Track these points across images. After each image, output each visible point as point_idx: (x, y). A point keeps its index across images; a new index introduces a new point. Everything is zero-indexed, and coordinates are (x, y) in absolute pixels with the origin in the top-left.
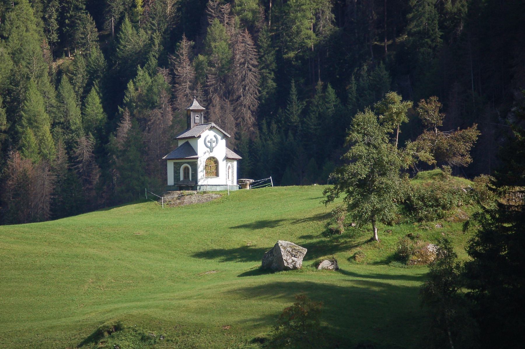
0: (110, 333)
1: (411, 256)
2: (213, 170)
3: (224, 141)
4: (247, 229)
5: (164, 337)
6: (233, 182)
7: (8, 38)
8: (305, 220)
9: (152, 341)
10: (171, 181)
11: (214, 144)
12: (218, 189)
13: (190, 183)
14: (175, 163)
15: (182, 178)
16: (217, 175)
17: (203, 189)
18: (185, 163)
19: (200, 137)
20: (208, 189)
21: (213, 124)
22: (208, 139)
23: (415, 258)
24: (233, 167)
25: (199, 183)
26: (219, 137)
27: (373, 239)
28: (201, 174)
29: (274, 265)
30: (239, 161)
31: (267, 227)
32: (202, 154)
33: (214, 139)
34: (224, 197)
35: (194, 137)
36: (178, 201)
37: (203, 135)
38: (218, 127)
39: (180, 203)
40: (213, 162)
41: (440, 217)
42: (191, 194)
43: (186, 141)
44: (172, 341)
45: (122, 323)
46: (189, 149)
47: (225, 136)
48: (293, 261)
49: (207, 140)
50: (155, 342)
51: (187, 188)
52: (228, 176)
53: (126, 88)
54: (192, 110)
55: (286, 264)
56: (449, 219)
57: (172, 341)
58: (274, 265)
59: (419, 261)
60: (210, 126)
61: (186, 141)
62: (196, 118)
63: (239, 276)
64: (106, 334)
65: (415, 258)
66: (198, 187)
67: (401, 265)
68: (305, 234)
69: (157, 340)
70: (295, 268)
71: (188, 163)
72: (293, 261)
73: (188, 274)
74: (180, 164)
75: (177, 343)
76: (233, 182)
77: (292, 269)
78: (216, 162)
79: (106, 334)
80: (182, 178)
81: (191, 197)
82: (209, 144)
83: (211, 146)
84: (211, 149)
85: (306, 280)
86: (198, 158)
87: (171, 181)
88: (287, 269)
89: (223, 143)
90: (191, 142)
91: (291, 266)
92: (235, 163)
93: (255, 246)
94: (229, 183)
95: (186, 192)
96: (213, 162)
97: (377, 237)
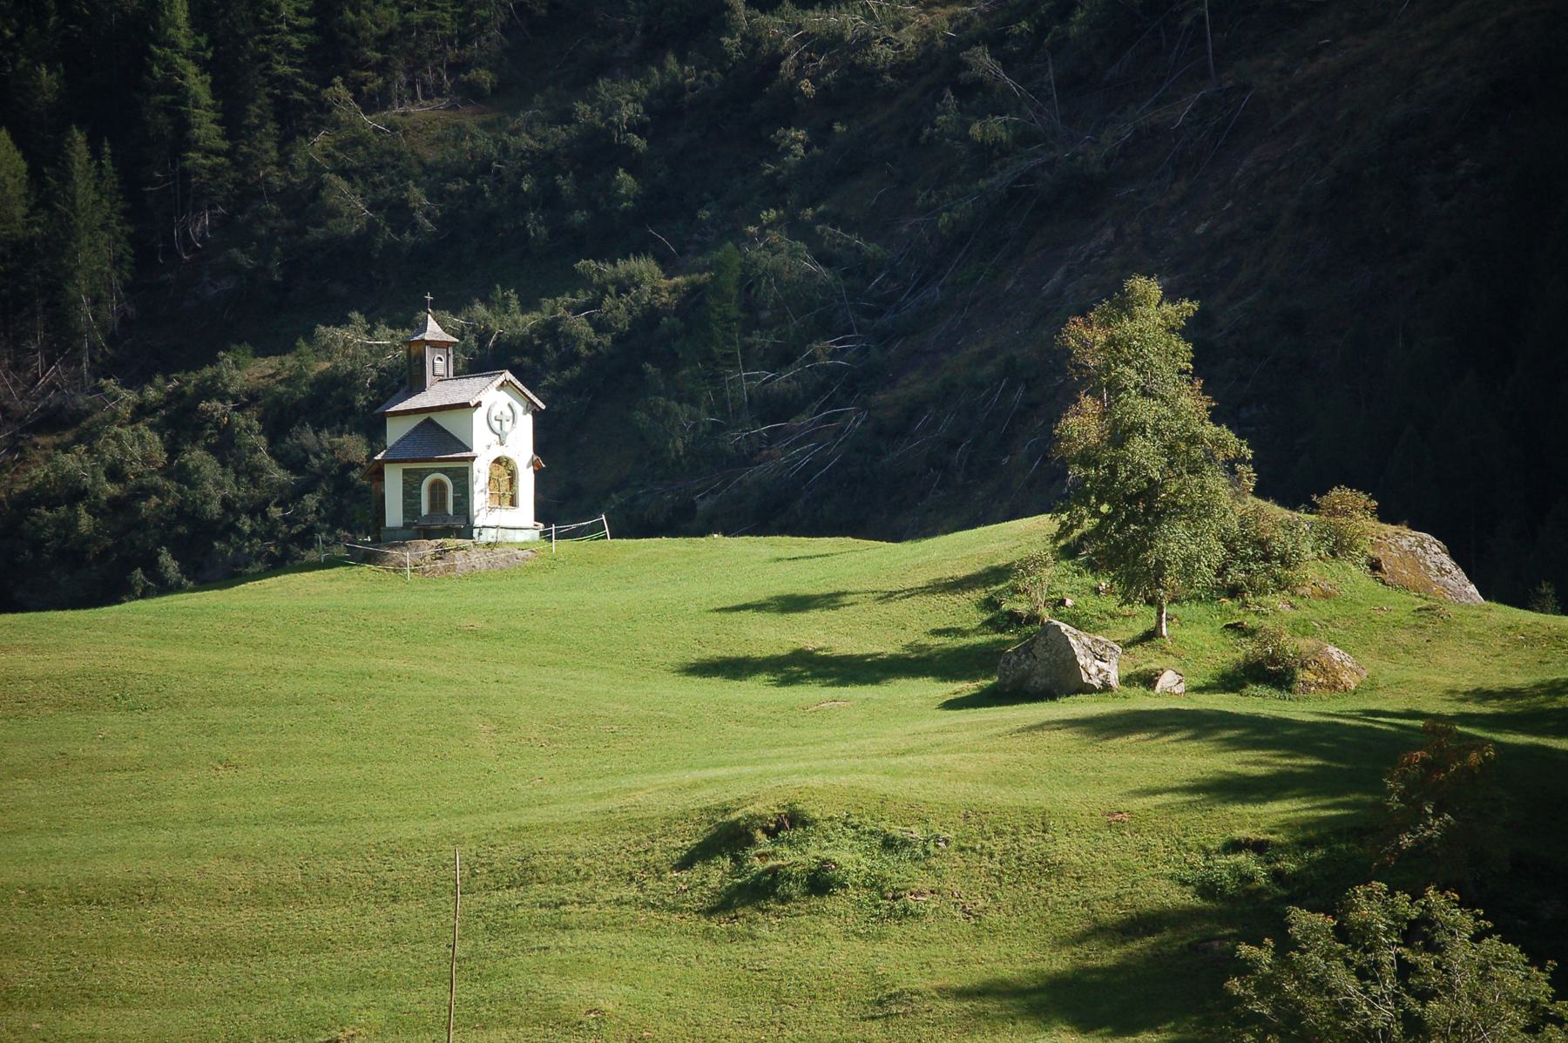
0: (771, 834)
1: (1299, 671)
3: (529, 417)
4: (758, 616)
5: (946, 842)
8: (912, 593)
9: (919, 851)
13: (462, 526)
14: (405, 472)
15: (425, 509)
16: (513, 502)
17: (489, 536)
19: (478, 405)
21: (508, 375)
23: (1310, 676)
25: (478, 522)
26: (519, 408)
28: (480, 499)
31: (815, 607)
35: (465, 405)
36: (440, 564)
38: (518, 384)
39: (447, 569)
41: (1281, 585)
44: (974, 850)
45: (800, 807)
48: (1100, 671)
50: (927, 853)
51: (447, 532)
54: (428, 343)
55: (1085, 678)
56: (1301, 592)
57: (974, 850)
59: (1320, 685)
61: (425, 416)
64: (760, 836)
65: (1310, 676)
66: (476, 532)
67: (1277, 694)
68: (941, 626)
69: (931, 847)
70: (1106, 687)
71: (444, 471)
72: (1100, 671)
73: (242, 748)
74: (422, 474)
75: (991, 856)
77: (1100, 691)
79: (760, 836)
80: (425, 509)
81: (466, 556)
82: (496, 425)
85: (1274, 713)
87: (394, 515)
88: (1088, 689)
91: (1096, 682)
93: (829, 649)
95: (452, 542)
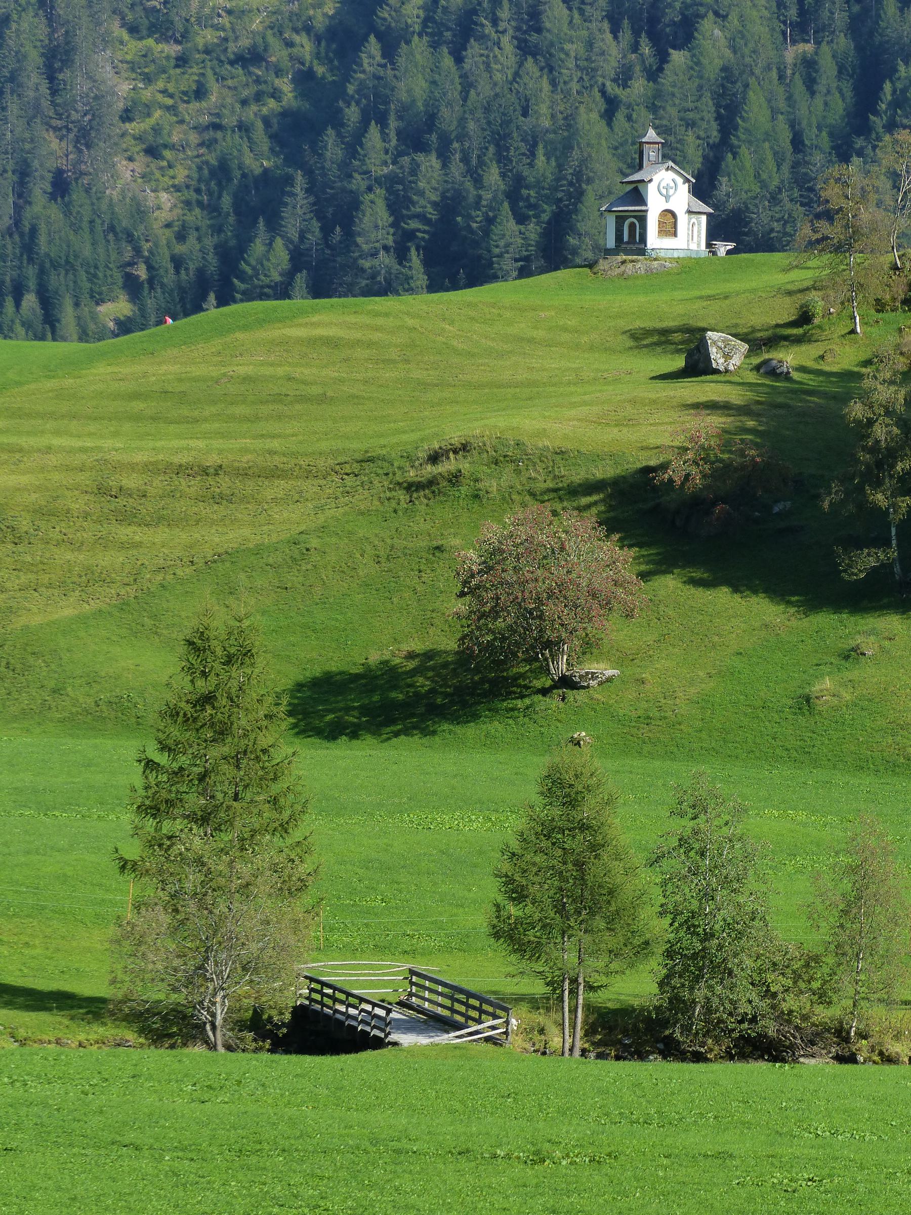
2: (669, 228)
6: (699, 245)
7: (727, 16)
10: (611, 243)
11: (671, 192)
12: (676, 254)
14: (617, 217)
18: (631, 217)
19: (651, 181)
20: (662, 254)
22: (663, 184)
24: (699, 224)
26: (680, 180)
27: (853, 331)
29: (701, 365)
30: (709, 215)
32: (655, 205)
33: (672, 184)
34: (687, 268)
35: (643, 181)
37: (656, 178)
38: (677, 168)
40: (669, 215)
42: (633, 261)
43: (633, 186)
46: (637, 195)
47: (687, 180)
49: (663, 184)
52: (692, 237)
53: (882, 89)
55: (714, 366)
58: (701, 365)
60: (666, 165)
61: (633, 186)
62: (651, 154)
63: (653, 378)
70: (727, 371)
71: (635, 217)
76: (699, 245)
78: (673, 215)
80: (626, 238)
82: (664, 191)
83: (667, 191)
84: (667, 198)
86: (646, 211)
88: (716, 372)
89: (684, 189)
90: (640, 186)
91: (722, 368)
92: (704, 218)
94: (693, 246)
96: (669, 215)
97: (859, 330)
